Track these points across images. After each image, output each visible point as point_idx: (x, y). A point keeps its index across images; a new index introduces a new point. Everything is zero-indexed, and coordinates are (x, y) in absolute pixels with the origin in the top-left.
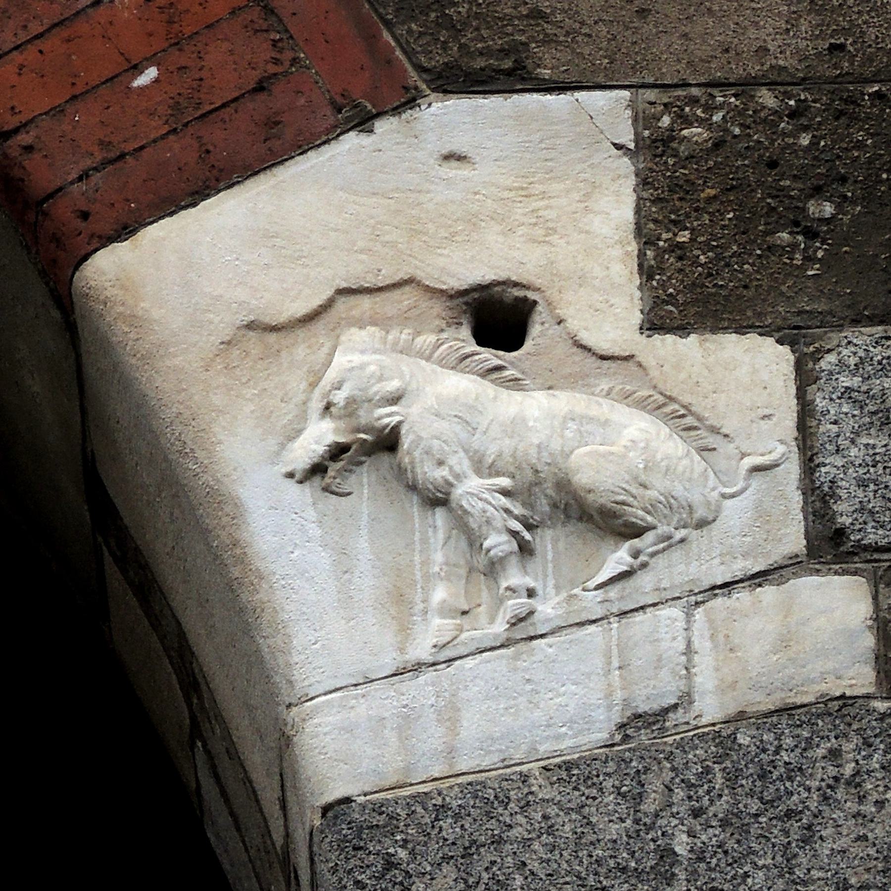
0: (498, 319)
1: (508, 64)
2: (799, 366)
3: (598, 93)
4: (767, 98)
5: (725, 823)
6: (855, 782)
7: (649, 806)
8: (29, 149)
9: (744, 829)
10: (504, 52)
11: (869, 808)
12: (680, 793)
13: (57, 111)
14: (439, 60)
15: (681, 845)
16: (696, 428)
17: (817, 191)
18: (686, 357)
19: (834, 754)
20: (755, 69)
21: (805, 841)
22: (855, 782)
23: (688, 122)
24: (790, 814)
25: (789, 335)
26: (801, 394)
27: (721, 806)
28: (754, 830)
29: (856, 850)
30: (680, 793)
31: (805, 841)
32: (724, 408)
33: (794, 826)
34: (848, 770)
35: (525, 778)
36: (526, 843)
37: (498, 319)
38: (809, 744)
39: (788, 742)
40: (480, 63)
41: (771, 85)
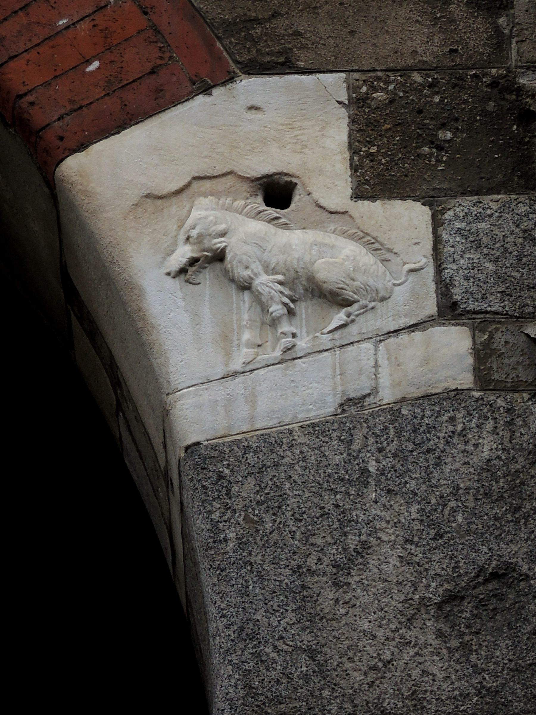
0: (277, 193)
1: (282, 59)
2: (434, 217)
4: (417, 77)
5: (395, 456)
6: (463, 434)
7: (355, 447)
8: (32, 104)
10: (280, 53)
11: (470, 448)
12: (371, 440)
13: (47, 84)
14: (246, 57)
15: (372, 467)
17: (443, 126)
19: (452, 419)
21: (437, 464)
22: (463, 434)
24: (429, 451)
25: (428, 201)
26: (435, 232)
27: (393, 447)
30: (371, 440)
34: (459, 427)
35: (291, 432)
36: (292, 466)
37: (277, 193)
39: (428, 413)
40: (267, 59)
41: (419, 70)
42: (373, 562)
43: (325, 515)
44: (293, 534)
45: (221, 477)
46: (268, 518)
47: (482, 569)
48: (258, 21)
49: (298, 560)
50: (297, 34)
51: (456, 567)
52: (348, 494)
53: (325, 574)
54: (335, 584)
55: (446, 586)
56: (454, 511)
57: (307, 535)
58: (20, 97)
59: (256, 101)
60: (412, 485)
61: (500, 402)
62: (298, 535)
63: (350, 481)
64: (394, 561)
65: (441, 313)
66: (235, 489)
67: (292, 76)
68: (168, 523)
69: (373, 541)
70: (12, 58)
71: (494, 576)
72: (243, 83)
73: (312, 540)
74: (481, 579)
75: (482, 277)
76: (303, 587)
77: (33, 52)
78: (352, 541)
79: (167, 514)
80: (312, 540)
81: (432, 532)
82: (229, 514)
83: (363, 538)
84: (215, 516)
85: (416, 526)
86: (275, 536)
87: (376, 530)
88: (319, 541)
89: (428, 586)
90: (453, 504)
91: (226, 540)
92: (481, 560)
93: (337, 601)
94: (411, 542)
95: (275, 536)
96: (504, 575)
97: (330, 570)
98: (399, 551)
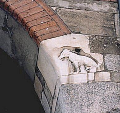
0: (78, 51)
1: (78, 32)
2: (103, 56)
3: (55, 38)
4: (101, 37)
5: (98, 90)
6: (109, 88)
7: (91, 88)
8: (37, 33)
9: (99, 90)
10: (78, 31)
11: (110, 90)
12: (93, 87)
13: (39, 30)
14: (72, 31)
15: (94, 91)
16: (40, 18)
17: (105, 44)
18: (93, 55)
19: (107, 86)
20: (99, 35)
21: (105, 92)
22: (109, 88)
23: (94, 38)
24: (103, 90)
25: (103, 54)
26: (104, 59)
27: (97, 88)
28: (100, 90)
29: (109, 93)
30: (93, 87)
31: (105, 92)
32: (98, 60)
33: (104, 90)
34: (108, 87)
35: (80, 84)
36: (80, 89)
37: (78, 51)
38: (105, 85)
39: (103, 84)
40: (76, 32)
41: (101, 36)
42: (94, 105)
43: (86, 97)
44: (80, 100)
45: (68, 89)
46: (76, 97)
47: (113, 108)
48: (75, 26)
49: (80, 104)
50: (81, 29)
51: (109, 108)
52: (90, 95)
53: (85, 106)
54: (88, 108)
55: (107, 110)
56: (108, 99)
57: (83, 100)
58: (35, 31)
59: (74, 37)
60: (101, 94)
61: (115, 84)
62: (81, 100)
63: (90, 93)
64: (97, 106)
65: (105, 70)
66: (70, 91)
67: (106, 72)
68: (51, 107)
69: (94, 102)
70: (33, 26)
71: (115, 110)
72: (88, 48)
73: (84, 101)
74: (113, 110)
75: (112, 66)
76: (82, 108)
77: (37, 26)
78: (90, 102)
79: (51, 106)
80: (84, 101)
81: (104, 102)
82: (69, 95)
83: (92, 101)
84: (67, 95)
85: (101, 100)
86: (77, 100)
87: (94, 100)
88: (85, 101)
89: (104, 110)
90: (108, 98)
91: (68, 99)
92: (113, 107)
93: (88, 110)
94: (100, 103)
95: (77, 100)
96: (117, 110)
97: (87, 106)
98: (98, 104)
